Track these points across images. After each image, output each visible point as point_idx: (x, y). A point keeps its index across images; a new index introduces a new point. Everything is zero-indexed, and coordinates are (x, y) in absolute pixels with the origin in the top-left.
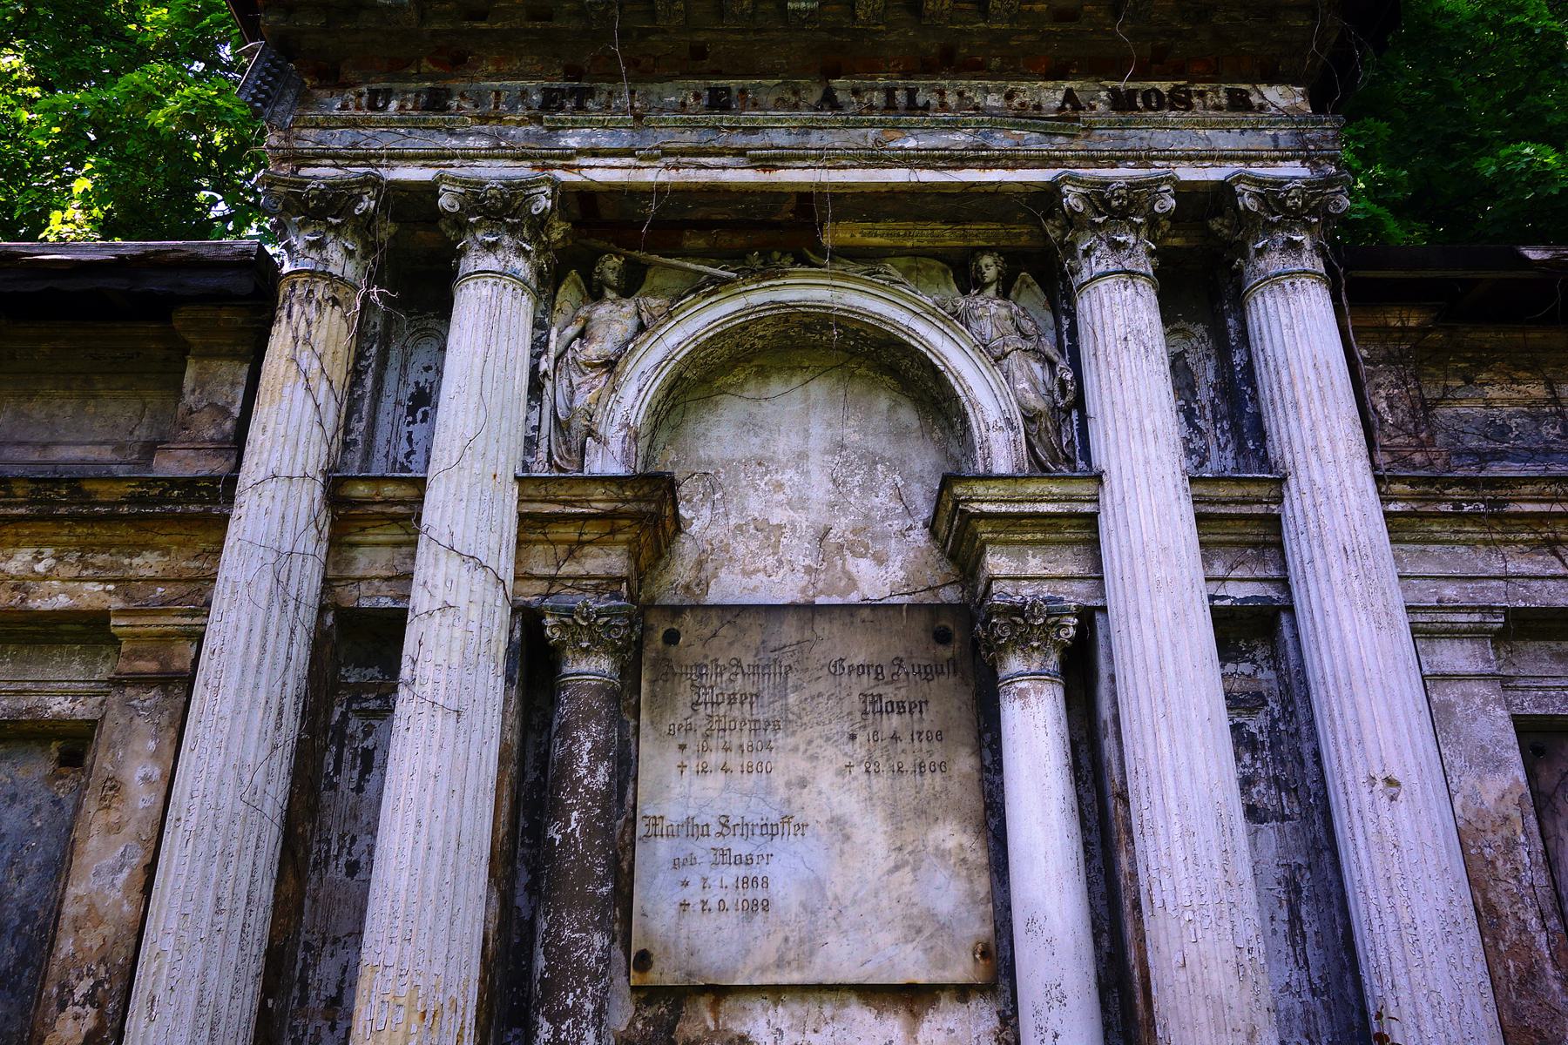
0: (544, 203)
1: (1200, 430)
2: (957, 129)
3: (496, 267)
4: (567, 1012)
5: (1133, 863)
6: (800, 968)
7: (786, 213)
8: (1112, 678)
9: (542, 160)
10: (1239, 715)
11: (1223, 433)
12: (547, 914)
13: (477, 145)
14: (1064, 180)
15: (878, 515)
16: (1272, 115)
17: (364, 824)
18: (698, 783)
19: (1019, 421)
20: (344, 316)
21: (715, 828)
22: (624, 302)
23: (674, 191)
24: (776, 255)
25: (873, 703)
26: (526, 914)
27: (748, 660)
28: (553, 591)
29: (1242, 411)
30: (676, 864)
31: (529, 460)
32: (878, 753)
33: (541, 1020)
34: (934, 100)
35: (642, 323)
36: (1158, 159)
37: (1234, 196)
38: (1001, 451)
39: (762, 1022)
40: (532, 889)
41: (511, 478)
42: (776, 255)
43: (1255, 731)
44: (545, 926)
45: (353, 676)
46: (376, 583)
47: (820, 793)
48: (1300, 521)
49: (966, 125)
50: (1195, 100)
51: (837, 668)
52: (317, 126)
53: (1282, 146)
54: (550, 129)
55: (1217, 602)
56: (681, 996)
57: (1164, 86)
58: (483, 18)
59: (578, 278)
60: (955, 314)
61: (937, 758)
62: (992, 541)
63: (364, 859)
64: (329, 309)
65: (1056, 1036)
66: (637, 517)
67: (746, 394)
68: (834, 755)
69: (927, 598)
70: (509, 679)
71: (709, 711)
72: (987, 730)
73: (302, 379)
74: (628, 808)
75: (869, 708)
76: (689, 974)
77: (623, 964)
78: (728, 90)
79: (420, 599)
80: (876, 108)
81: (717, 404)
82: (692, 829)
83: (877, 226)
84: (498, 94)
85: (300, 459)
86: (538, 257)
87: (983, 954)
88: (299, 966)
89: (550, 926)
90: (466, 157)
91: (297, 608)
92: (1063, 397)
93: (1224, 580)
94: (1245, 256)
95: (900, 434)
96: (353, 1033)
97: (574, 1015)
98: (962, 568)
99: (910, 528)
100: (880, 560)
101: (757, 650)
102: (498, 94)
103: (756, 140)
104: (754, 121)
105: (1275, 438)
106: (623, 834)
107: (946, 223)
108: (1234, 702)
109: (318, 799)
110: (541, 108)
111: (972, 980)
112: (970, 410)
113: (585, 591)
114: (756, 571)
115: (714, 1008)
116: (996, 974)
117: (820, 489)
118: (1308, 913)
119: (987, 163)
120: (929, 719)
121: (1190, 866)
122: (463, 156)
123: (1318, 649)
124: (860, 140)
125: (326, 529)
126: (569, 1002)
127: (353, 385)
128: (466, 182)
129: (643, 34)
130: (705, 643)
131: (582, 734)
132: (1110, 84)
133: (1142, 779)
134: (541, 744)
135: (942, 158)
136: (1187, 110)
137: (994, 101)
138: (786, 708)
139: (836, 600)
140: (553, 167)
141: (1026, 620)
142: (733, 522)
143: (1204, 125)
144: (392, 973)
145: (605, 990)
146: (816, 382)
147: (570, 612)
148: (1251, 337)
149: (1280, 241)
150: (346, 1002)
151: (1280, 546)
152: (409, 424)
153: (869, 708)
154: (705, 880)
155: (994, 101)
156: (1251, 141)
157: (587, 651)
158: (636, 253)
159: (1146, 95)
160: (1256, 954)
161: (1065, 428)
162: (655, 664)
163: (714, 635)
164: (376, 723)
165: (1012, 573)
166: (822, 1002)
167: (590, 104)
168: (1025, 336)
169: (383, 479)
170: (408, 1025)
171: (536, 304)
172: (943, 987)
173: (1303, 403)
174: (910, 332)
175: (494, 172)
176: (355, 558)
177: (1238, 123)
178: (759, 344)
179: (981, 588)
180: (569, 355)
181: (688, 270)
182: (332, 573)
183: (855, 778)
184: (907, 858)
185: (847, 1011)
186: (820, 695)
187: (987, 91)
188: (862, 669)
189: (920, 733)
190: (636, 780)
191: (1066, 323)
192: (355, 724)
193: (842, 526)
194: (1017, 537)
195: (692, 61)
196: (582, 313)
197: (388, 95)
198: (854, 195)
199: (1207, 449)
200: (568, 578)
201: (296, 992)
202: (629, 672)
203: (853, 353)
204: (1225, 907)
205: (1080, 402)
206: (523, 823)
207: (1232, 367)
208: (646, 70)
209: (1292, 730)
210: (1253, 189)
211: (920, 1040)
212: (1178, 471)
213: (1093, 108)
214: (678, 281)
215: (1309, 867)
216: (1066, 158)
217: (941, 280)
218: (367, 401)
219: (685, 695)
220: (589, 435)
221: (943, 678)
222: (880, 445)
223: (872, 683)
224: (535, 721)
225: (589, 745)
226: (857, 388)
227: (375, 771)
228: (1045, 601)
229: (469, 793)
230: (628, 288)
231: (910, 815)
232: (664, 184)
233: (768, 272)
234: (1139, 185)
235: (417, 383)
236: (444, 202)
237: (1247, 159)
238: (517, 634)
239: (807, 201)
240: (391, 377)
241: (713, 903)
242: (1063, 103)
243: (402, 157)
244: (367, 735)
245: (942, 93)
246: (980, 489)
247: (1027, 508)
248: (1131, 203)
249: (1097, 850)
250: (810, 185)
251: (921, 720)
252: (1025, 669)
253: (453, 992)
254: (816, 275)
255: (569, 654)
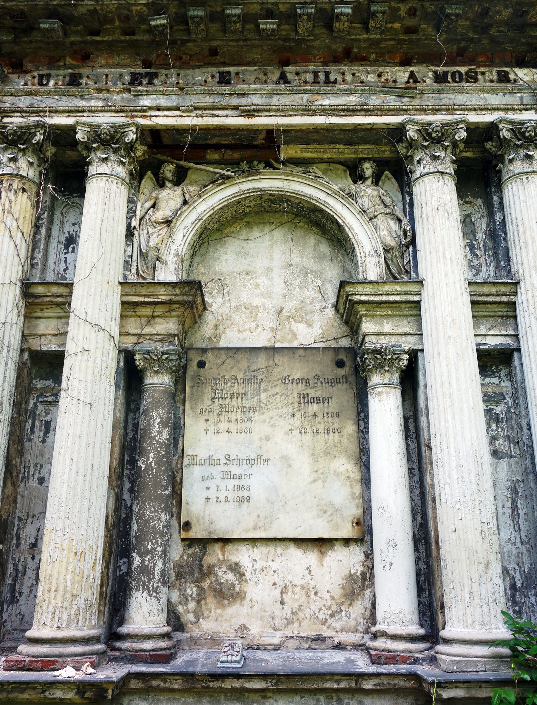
0: (131, 137)
1: (477, 255)
2: (352, 94)
3: (108, 171)
4: (148, 552)
5: (432, 480)
6: (265, 530)
7: (260, 140)
8: (425, 386)
9: (130, 112)
10: (491, 404)
11: (489, 257)
12: (138, 504)
13: (96, 105)
14: (407, 122)
15: (308, 301)
16: (521, 85)
17: (45, 460)
18: (215, 437)
19: (381, 252)
20: (29, 198)
21: (223, 461)
22: (176, 188)
23: (201, 129)
24: (256, 163)
25: (304, 398)
26: (129, 503)
27: (240, 376)
28: (140, 341)
29: (499, 246)
30: (203, 479)
31: (127, 273)
32: (306, 423)
33: (136, 555)
34: (339, 78)
35: (185, 199)
36: (458, 110)
37: (498, 130)
38: (372, 268)
39: (246, 556)
40: (131, 491)
41: (117, 283)
42: (256, 163)
43: (499, 413)
44: (137, 510)
45: (39, 384)
46: (49, 337)
47: (276, 443)
48: (525, 305)
49: (356, 92)
50: (480, 77)
51: (286, 380)
52: (11, 95)
53: (525, 102)
54: (135, 96)
55: (481, 347)
56: (204, 543)
57: (463, 69)
58: (97, 34)
59: (152, 176)
60: (350, 195)
61: (336, 426)
62: (366, 316)
63: (46, 476)
64: (21, 194)
65: (391, 564)
66: (183, 304)
67: (240, 237)
68: (285, 424)
69: (333, 344)
70: (117, 386)
71: (220, 402)
72: (362, 411)
73: (8, 232)
74: (179, 450)
75: (302, 401)
76: (210, 533)
77: (177, 527)
78: (229, 73)
79: (70, 348)
80: (308, 83)
81: (225, 242)
82: (212, 461)
83: (309, 147)
84: (107, 76)
85: (8, 274)
86: (130, 165)
87: (357, 524)
88: (15, 529)
89: (140, 510)
90: (90, 111)
91: (8, 351)
92: (405, 239)
93: (485, 335)
94: (503, 163)
95: (320, 258)
96: (42, 562)
97: (152, 553)
98: (351, 328)
99: (325, 308)
100: (309, 324)
101: (245, 370)
102: (107, 76)
103: (244, 101)
104: (243, 90)
105: (515, 261)
106: (177, 464)
107: (345, 145)
108: (488, 398)
109: (23, 445)
110: (130, 84)
111: (351, 536)
112: (356, 246)
113: (156, 341)
114: (245, 330)
115: (223, 549)
116: (363, 534)
117: (279, 287)
118: (521, 504)
119: (368, 112)
120: (333, 407)
121: (460, 482)
122: (93, 108)
123: (531, 371)
124: (299, 101)
125: (23, 310)
126: (149, 547)
127: (35, 233)
128: (91, 125)
129: (184, 42)
130: (218, 367)
131: (155, 414)
132: (434, 68)
133: (438, 438)
134: (135, 419)
135: (343, 110)
136: (475, 82)
137: (371, 78)
138: (260, 401)
139: (287, 345)
140: (136, 117)
141: (382, 356)
142: (233, 304)
143: (483, 91)
144: (59, 533)
145: (168, 541)
146: (277, 230)
147: (148, 352)
148: (505, 207)
149: (522, 155)
150: (39, 547)
151: (515, 317)
152: (65, 253)
153: (302, 401)
154: (218, 486)
155: (371, 78)
156: (509, 100)
157: (157, 372)
158: (182, 163)
159: (453, 74)
160: (491, 525)
161: (406, 255)
162: (193, 378)
163: (223, 363)
164: (51, 408)
165: (376, 332)
166: (276, 546)
167: (156, 81)
168: (386, 206)
169: (52, 283)
170: (68, 559)
171: (129, 191)
172: (336, 540)
173: (530, 243)
174: (326, 204)
175: (106, 120)
176: (38, 325)
177: (502, 90)
178: (247, 210)
179: (360, 339)
180: (147, 217)
181: (209, 171)
182: (26, 332)
183: (294, 436)
184: (320, 476)
185: (288, 551)
186: (277, 394)
187: (368, 72)
188: (299, 381)
189: (328, 413)
190: (183, 436)
191: (408, 199)
192: (41, 409)
193: (290, 306)
194: (378, 313)
195: (211, 57)
196: (154, 195)
197: (49, 76)
198: (296, 131)
199: (481, 266)
200: (148, 335)
201: (14, 541)
202: (180, 381)
203: (296, 215)
204: (477, 502)
205: (413, 242)
206: (127, 458)
207: (495, 222)
208: (184, 62)
209: (517, 412)
210: (508, 126)
211: (325, 565)
212: (463, 279)
213: (424, 81)
214: (205, 177)
215: (523, 481)
216: (409, 110)
217: (343, 176)
218: (43, 242)
219: (208, 394)
220: (158, 260)
221: (340, 385)
222: (310, 264)
223: (304, 388)
224: (132, 407)
225: (158, 420)
226: (299, 233)
227: (51, 432)
228: (392, 347)
229: (97, 445)
230: (180, 178)
231: (322, 454)
232: (196, 125)
233: (252, 172)
234: (447, 125)
235: (69, 232)
236: (80, 136)
237: (506, 110)
238: (122, 363)
239: (271, 133)
240: (55, 229)
241: (222, 498)
242: (409, 79)
243: (57, 112)
244: (47, 414)
245: (343, 74)
246: (359, 288)
247: (384, 298)
248: (443, 134)
249: (416, 472)
250: (273, 125)
251: (328, 407)
252: (381, 382)
253: (90, 542)
254: (276, 174)
255: (148, 374)
